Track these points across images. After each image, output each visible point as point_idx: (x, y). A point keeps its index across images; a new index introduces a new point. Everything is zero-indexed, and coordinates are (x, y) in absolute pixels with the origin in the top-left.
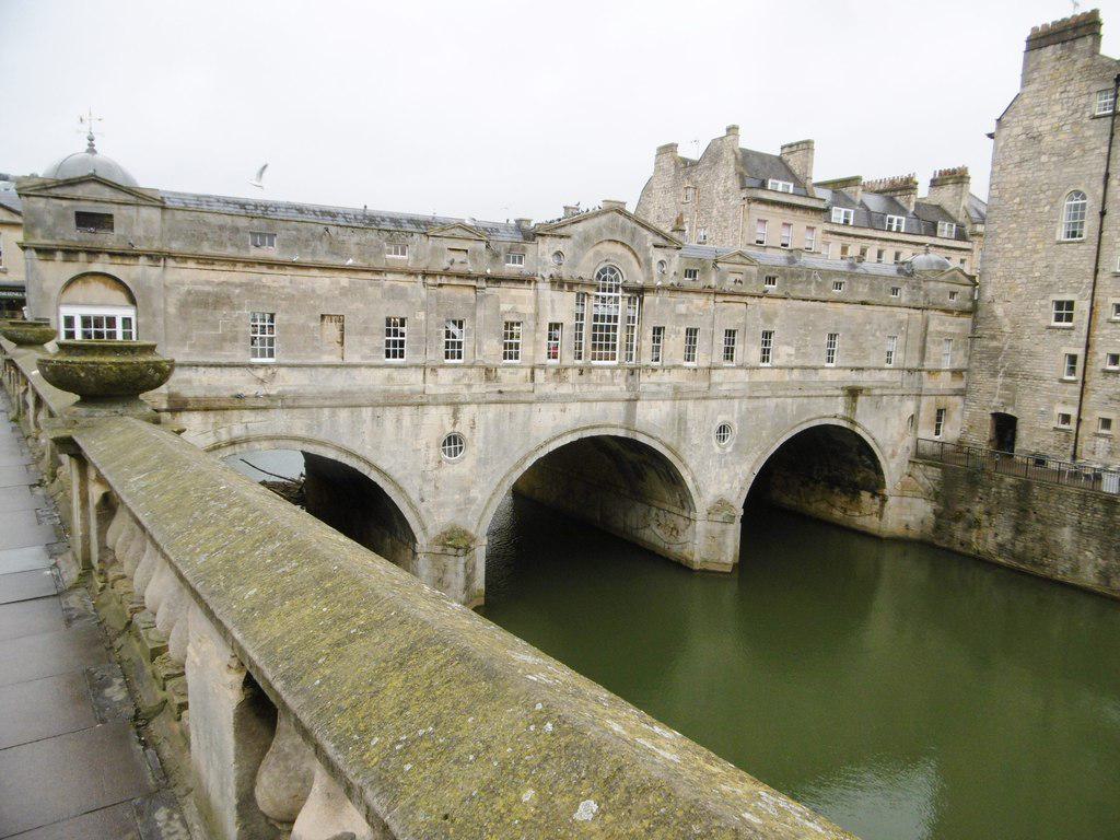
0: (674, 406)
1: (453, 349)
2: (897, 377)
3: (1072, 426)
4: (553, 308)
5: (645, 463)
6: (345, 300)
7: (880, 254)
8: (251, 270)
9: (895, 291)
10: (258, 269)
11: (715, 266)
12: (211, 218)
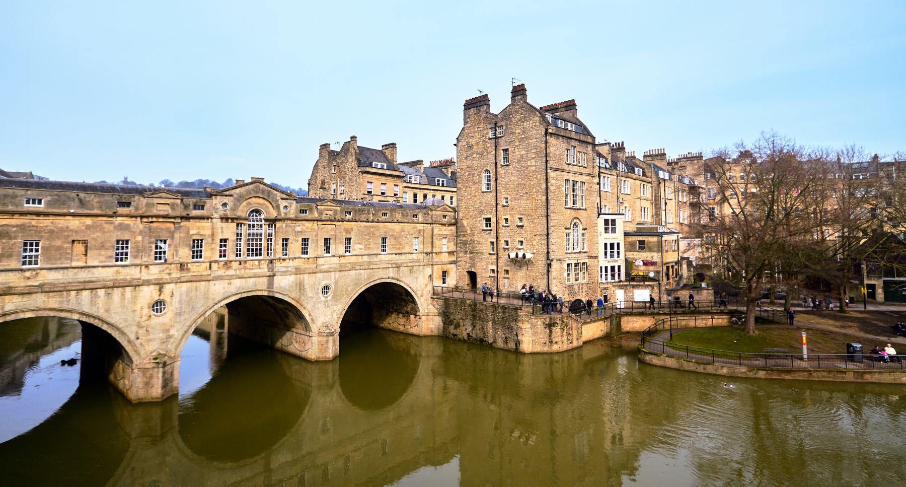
1: (159, 254)
2: (421, 256)
3: (496, 275)
5: (287, 309)
6: (89, 232)
9: (416, 216)
10: (29, 217)
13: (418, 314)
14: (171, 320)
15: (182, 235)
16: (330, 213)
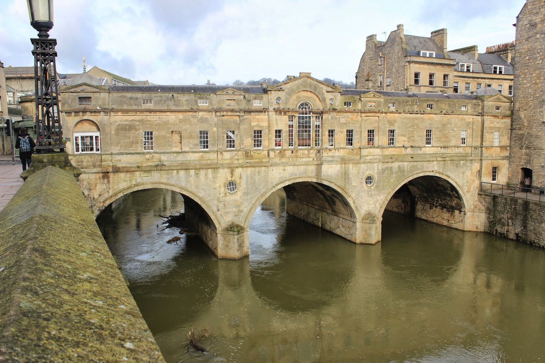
1: (231, 143)
5: (334, 196)
10: (145, 114)
14: (240, 198)
15: (246, 126)
16: (373, 104)
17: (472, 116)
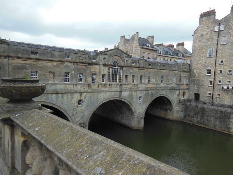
0: (130, 92)
1: (80, 80)
3: (212, 96)
4: (103, 71)
7: (171, 60)
8: (31, 60)
9: (174, 67)
11: (138, 62)
12: (21, 48)
13: (172, 110)
14: (85, 108)
17: (177, 71)
